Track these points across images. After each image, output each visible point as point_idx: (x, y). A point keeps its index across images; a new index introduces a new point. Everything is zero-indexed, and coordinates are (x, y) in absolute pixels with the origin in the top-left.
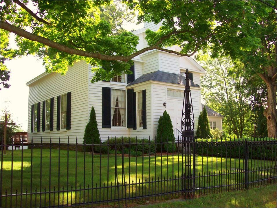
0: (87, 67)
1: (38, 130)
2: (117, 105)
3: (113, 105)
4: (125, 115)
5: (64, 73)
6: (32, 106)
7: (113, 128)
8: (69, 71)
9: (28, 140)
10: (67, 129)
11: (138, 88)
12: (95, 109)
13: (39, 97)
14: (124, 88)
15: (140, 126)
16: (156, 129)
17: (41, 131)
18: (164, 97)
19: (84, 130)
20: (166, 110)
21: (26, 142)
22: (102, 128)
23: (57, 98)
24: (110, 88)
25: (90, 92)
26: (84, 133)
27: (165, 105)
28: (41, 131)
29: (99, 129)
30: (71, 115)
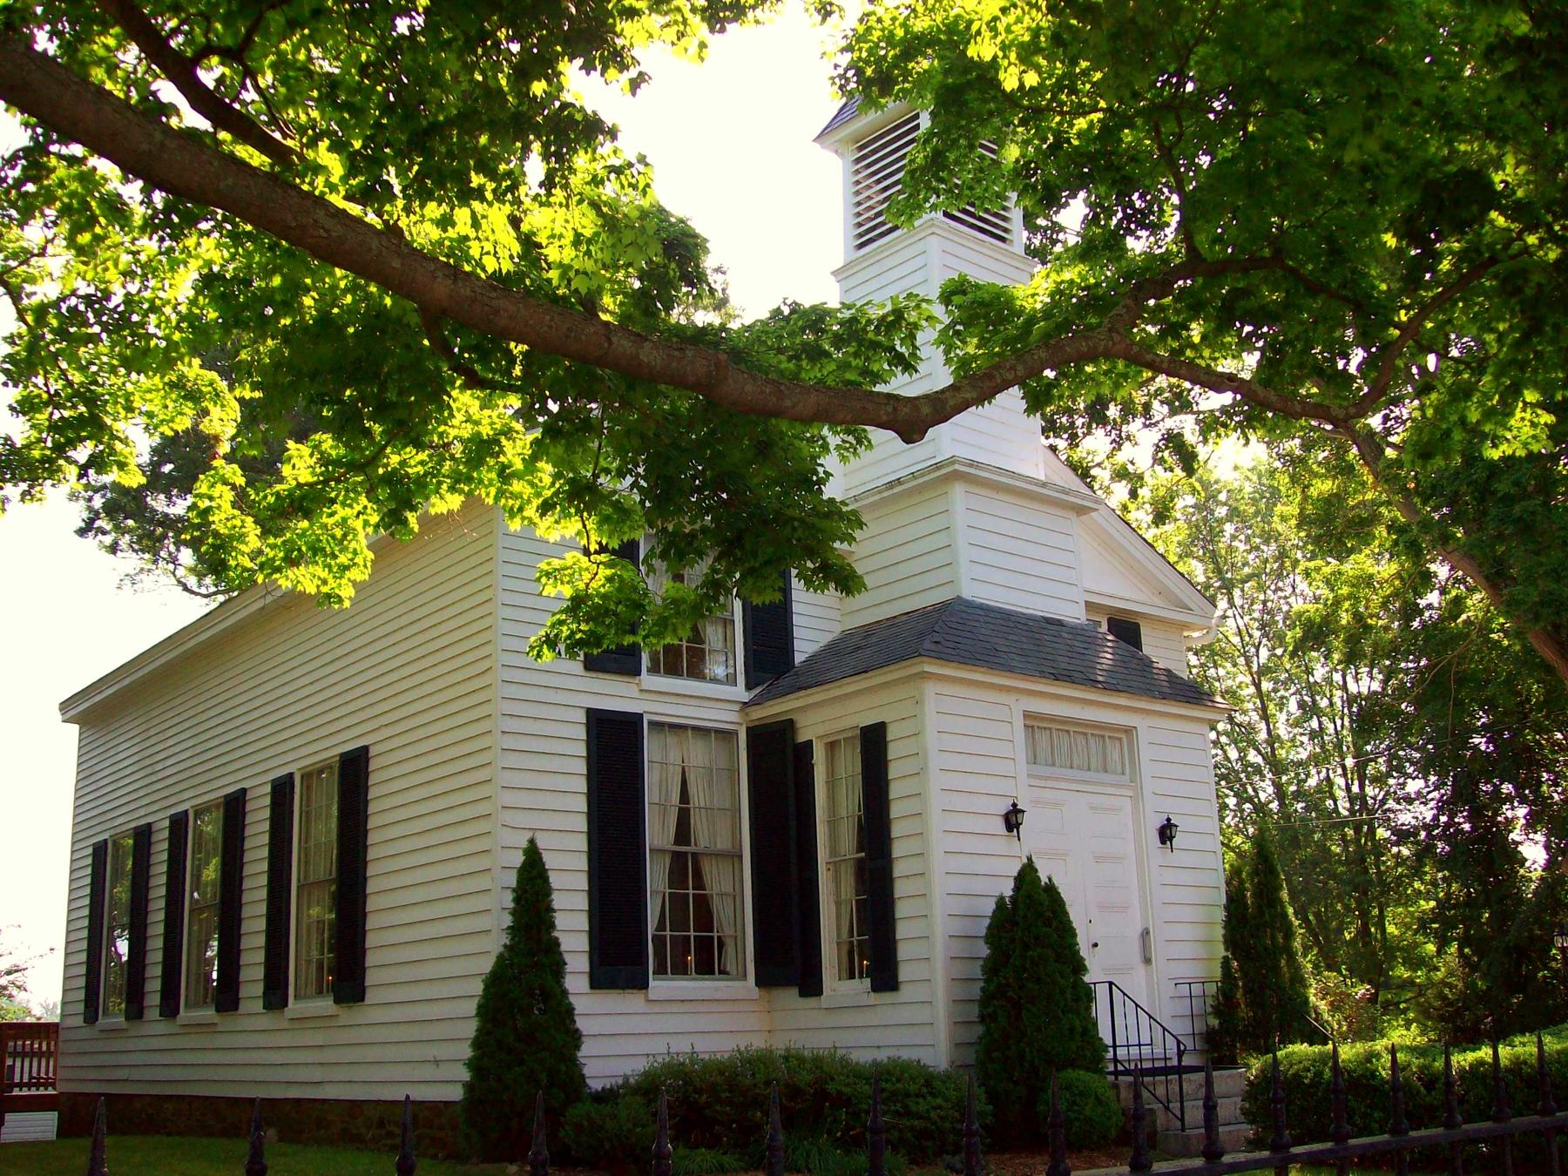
0: (535, 537)
1: (135, 1010)
2: (683, 832)
3: (657, 832)
4: (735, 896)
5: (343, 594)
6: (99, 851)
7: (659, 986)
8: (362, 606)
9: (62, 1074)
10: (218, 1010)
11: (823, 718)
12: (549, 860)
13: (141, 793)
14: (726, 717)
15: (844, 975)
16: (976, 991)
17: (153, 1013)
18: (1006, 768)
19: (471, 1007)
20: (1030, 859)
21: (51, 1091)
22: (592, 987)
23: (268, 789)
24: (640, 716)
25: (509, 742)
26: (470, 1029)
27: (1018, 826)
28: (153, 1013)
29: (572, 999)
30: (372, 904)
